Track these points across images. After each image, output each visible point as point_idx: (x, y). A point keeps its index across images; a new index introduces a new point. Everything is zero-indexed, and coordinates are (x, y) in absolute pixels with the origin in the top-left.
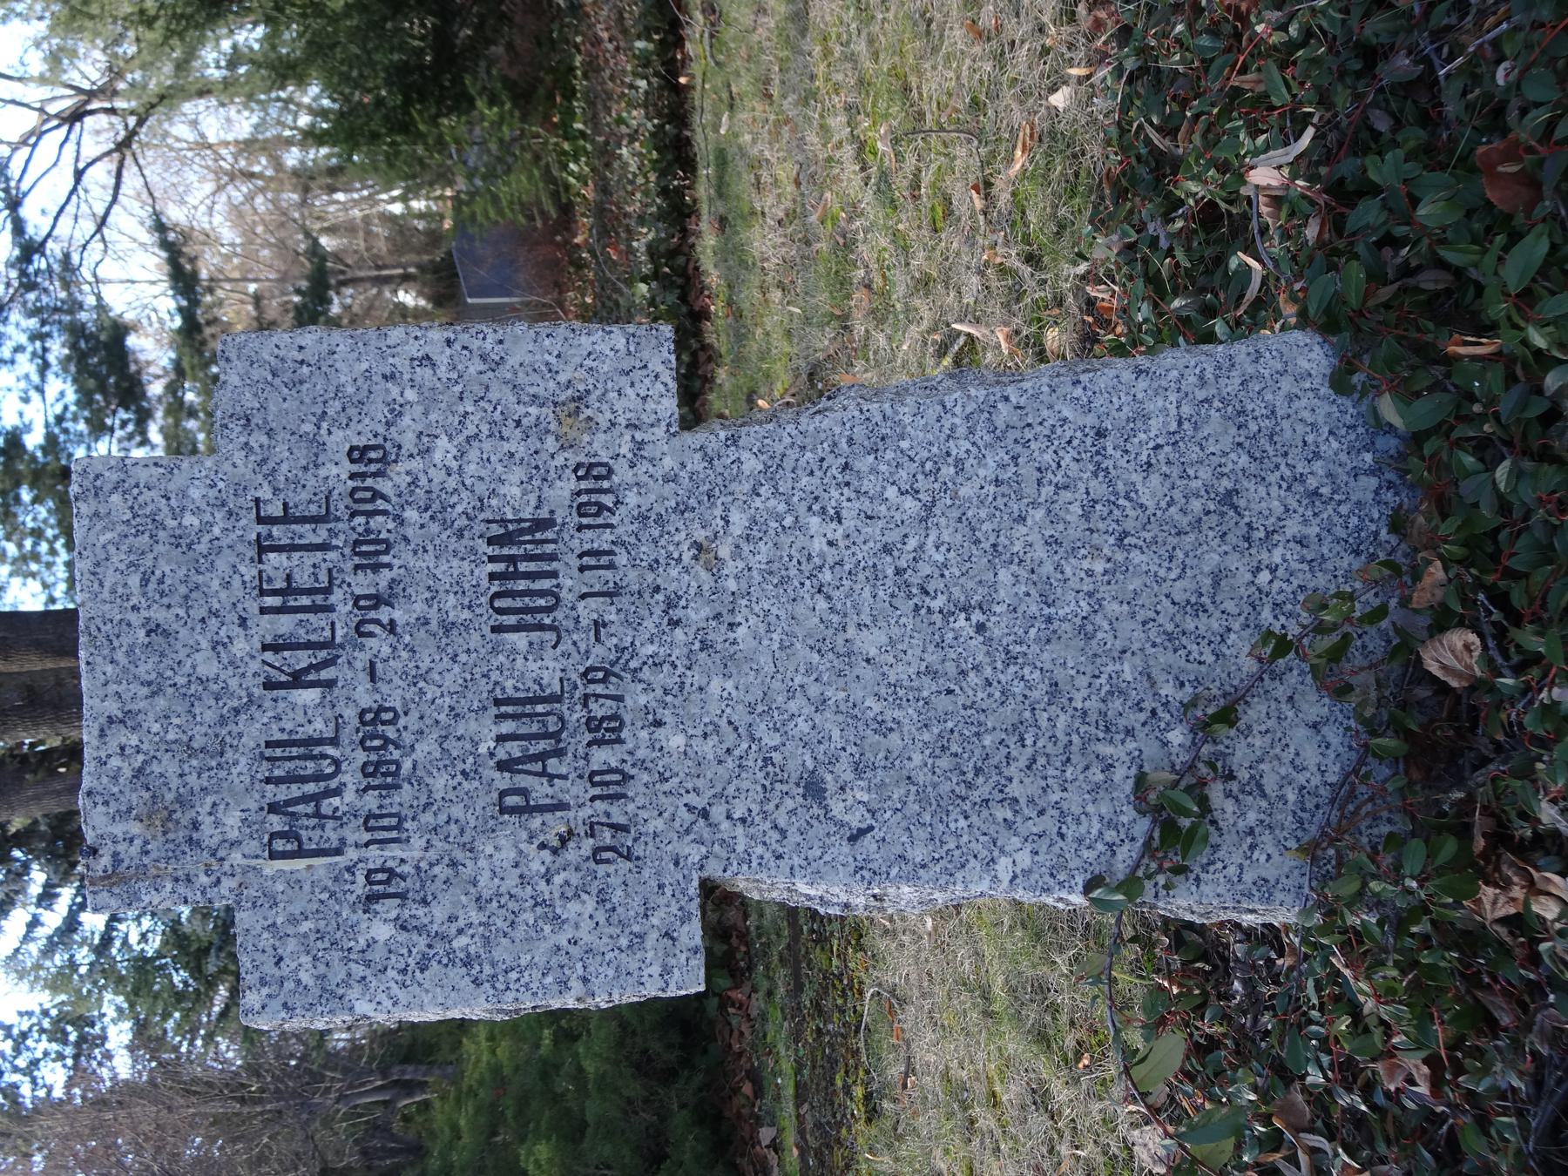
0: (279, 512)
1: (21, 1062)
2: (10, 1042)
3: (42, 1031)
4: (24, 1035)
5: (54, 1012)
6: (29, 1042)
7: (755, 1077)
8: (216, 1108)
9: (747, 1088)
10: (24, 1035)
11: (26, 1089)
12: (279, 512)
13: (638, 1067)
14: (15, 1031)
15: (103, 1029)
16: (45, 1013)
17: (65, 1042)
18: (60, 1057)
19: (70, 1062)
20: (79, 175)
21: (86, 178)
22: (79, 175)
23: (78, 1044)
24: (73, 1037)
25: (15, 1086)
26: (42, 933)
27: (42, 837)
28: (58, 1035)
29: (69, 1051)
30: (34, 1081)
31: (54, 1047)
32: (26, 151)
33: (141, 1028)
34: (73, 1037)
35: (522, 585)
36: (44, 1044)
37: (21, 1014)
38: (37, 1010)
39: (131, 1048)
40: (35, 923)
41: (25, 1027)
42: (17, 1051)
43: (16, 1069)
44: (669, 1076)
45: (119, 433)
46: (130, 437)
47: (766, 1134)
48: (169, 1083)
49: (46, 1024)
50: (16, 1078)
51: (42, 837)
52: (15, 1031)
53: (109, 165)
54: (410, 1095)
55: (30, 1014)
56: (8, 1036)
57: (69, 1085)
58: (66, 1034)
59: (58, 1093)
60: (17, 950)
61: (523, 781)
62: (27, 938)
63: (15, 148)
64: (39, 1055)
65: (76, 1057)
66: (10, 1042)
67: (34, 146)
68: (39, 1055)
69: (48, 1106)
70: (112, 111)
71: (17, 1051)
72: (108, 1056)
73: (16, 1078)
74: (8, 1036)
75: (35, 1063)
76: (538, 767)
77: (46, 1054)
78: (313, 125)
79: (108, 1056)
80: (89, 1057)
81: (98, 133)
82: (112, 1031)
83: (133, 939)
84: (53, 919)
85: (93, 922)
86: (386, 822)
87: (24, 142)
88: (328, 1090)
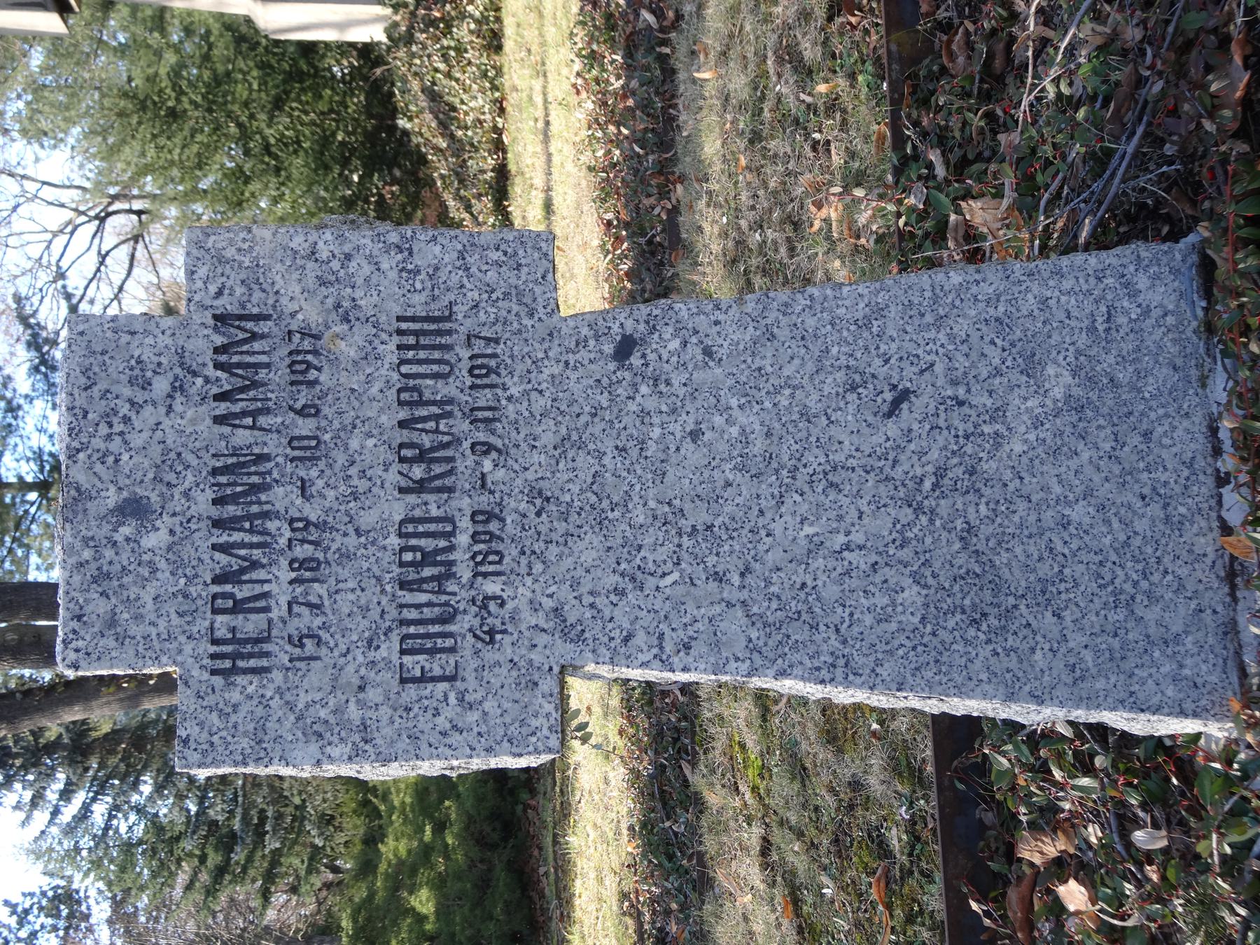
0: (418, 674)
2: (15, 918)
4: (26, 912)
5: (50, 894)
6: (30, 918)
7: (540, 849)
9: (536, 853)
10: (26, 912)
12: (418, 674)
13: (478, 841)
14: (20, 909)
15: (88, 908)
16: (44, 894)
17: (58, 916)
18: (55, 929)
19: (61, 933)
21: (108, 260)
22: (103, 257)
23: (69, 917)
24: (65, 913)
27: (64, 747)
29: (62, 924)
31: (50, 921)
32: (63, 239)
33: (117, 905)
34: (65, 913)
35: (422, 355)
36: (42, 919)
37: (24, 895)
38: (38, 892)
39: (110, 922)
41: (27, 906)
42: (21, 924)
44: (493, 847)
47: (542, 870)
49: (44, 903)
51: (64, 747)
52: (20, 909)
53: (125, 250)
55: (32, 895)
56: (14, 913)
58: (59, 911)
60: (43, 832)
61: (415, 437)
63: (55, 234)
64: (37, 927)
65: (67, 929)
66: (15, 918)
67: (72, 233)
68: (37, 927)
70: (130, 211)
74: (14, 913)
76: (249, 421)
77: (43, 927)
79: (90, 930)
80: (77, 929)
81: (120, 224)
82: (95, 909)
83: (123, 829)
84: (70, 811)
85: (100, 810)
87: (61, 231)
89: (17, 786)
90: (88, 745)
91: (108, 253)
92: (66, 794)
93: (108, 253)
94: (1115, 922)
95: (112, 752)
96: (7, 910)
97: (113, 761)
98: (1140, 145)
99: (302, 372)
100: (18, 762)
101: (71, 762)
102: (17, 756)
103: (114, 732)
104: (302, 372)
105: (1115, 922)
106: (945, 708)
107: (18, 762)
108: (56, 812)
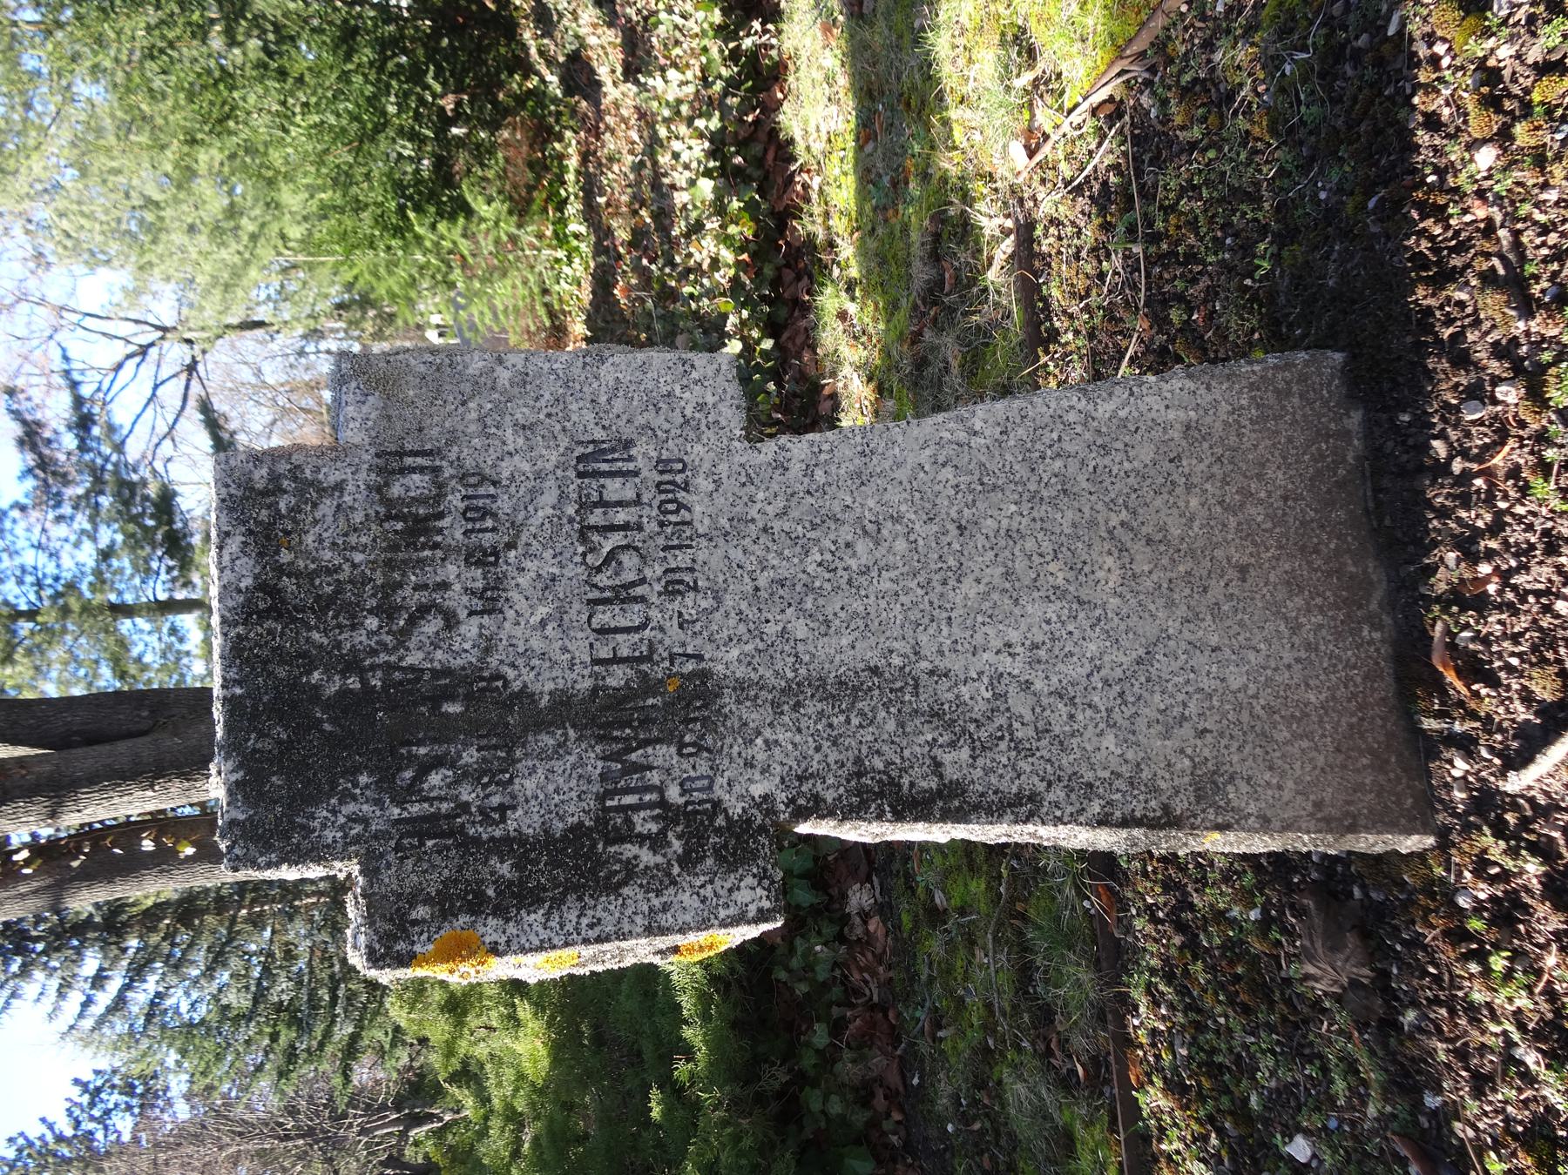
1: (96, 1113)
3: (113, 1087)
4: (98, 1090)
8: (252, 1146)
11: (100, 1135)
17: (132, 1094)
18: (129, 1108)
20: (156, 387)
25: (91, 1133)
26: (97, 1009)
27: (96, 927)
28: (129, 1089)
30: (106, 1128)
36: (116, 1097)
40: (88, 1002)
41: (99, 1083)
43: (92, 1119)
45: (163, 576)
46: (174, 580)
48: (218, 1121)
49: (116, 1081)
50: (91, 1126)
51: (96, 927)
54: (419, 1125)
57: (136, 1129)
59: (126, 1137)
62: (81, 1016)
65: (142, 1106)
69: (120, 1149)
71: (92, 1104)
72: (169, 1103)
73: (91, 1126)
74: (86, 1091)
75: (107, 1112)
78: (494, 773)
86: (699, 784)
88: (351, 1126)
89: (39, 975)
90: (125, 925)
91: (157, 328)
92: (99, 980)
93: (157, 328)
94: (134, 804)
95: (154, 929)
96: (78, 1089)
97: (154, 939)
98: (426, 960)
99: (474, 486)
100: (40, 947)
101: (105, 946)
102: (37, 939)
103: (156, 905)
104: (474, 486)
105: (134, 804)
106: (930, 838)
107: (40, 947)
108: (88, 1002)
